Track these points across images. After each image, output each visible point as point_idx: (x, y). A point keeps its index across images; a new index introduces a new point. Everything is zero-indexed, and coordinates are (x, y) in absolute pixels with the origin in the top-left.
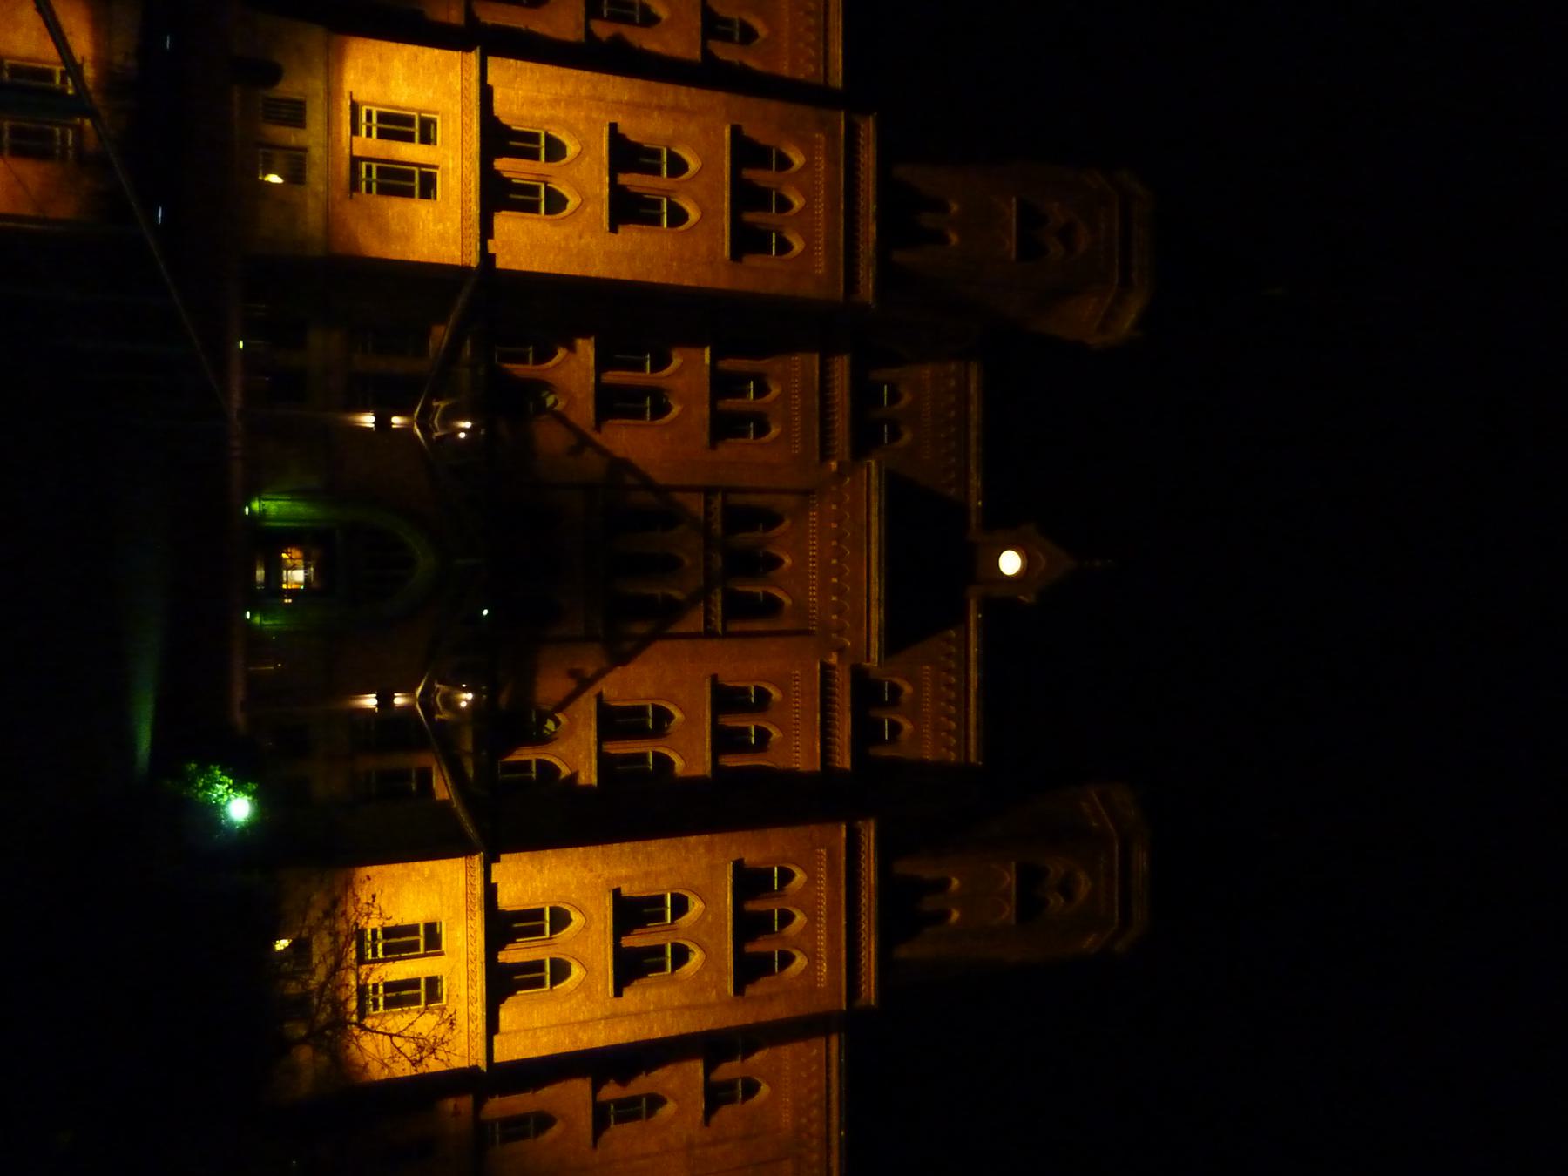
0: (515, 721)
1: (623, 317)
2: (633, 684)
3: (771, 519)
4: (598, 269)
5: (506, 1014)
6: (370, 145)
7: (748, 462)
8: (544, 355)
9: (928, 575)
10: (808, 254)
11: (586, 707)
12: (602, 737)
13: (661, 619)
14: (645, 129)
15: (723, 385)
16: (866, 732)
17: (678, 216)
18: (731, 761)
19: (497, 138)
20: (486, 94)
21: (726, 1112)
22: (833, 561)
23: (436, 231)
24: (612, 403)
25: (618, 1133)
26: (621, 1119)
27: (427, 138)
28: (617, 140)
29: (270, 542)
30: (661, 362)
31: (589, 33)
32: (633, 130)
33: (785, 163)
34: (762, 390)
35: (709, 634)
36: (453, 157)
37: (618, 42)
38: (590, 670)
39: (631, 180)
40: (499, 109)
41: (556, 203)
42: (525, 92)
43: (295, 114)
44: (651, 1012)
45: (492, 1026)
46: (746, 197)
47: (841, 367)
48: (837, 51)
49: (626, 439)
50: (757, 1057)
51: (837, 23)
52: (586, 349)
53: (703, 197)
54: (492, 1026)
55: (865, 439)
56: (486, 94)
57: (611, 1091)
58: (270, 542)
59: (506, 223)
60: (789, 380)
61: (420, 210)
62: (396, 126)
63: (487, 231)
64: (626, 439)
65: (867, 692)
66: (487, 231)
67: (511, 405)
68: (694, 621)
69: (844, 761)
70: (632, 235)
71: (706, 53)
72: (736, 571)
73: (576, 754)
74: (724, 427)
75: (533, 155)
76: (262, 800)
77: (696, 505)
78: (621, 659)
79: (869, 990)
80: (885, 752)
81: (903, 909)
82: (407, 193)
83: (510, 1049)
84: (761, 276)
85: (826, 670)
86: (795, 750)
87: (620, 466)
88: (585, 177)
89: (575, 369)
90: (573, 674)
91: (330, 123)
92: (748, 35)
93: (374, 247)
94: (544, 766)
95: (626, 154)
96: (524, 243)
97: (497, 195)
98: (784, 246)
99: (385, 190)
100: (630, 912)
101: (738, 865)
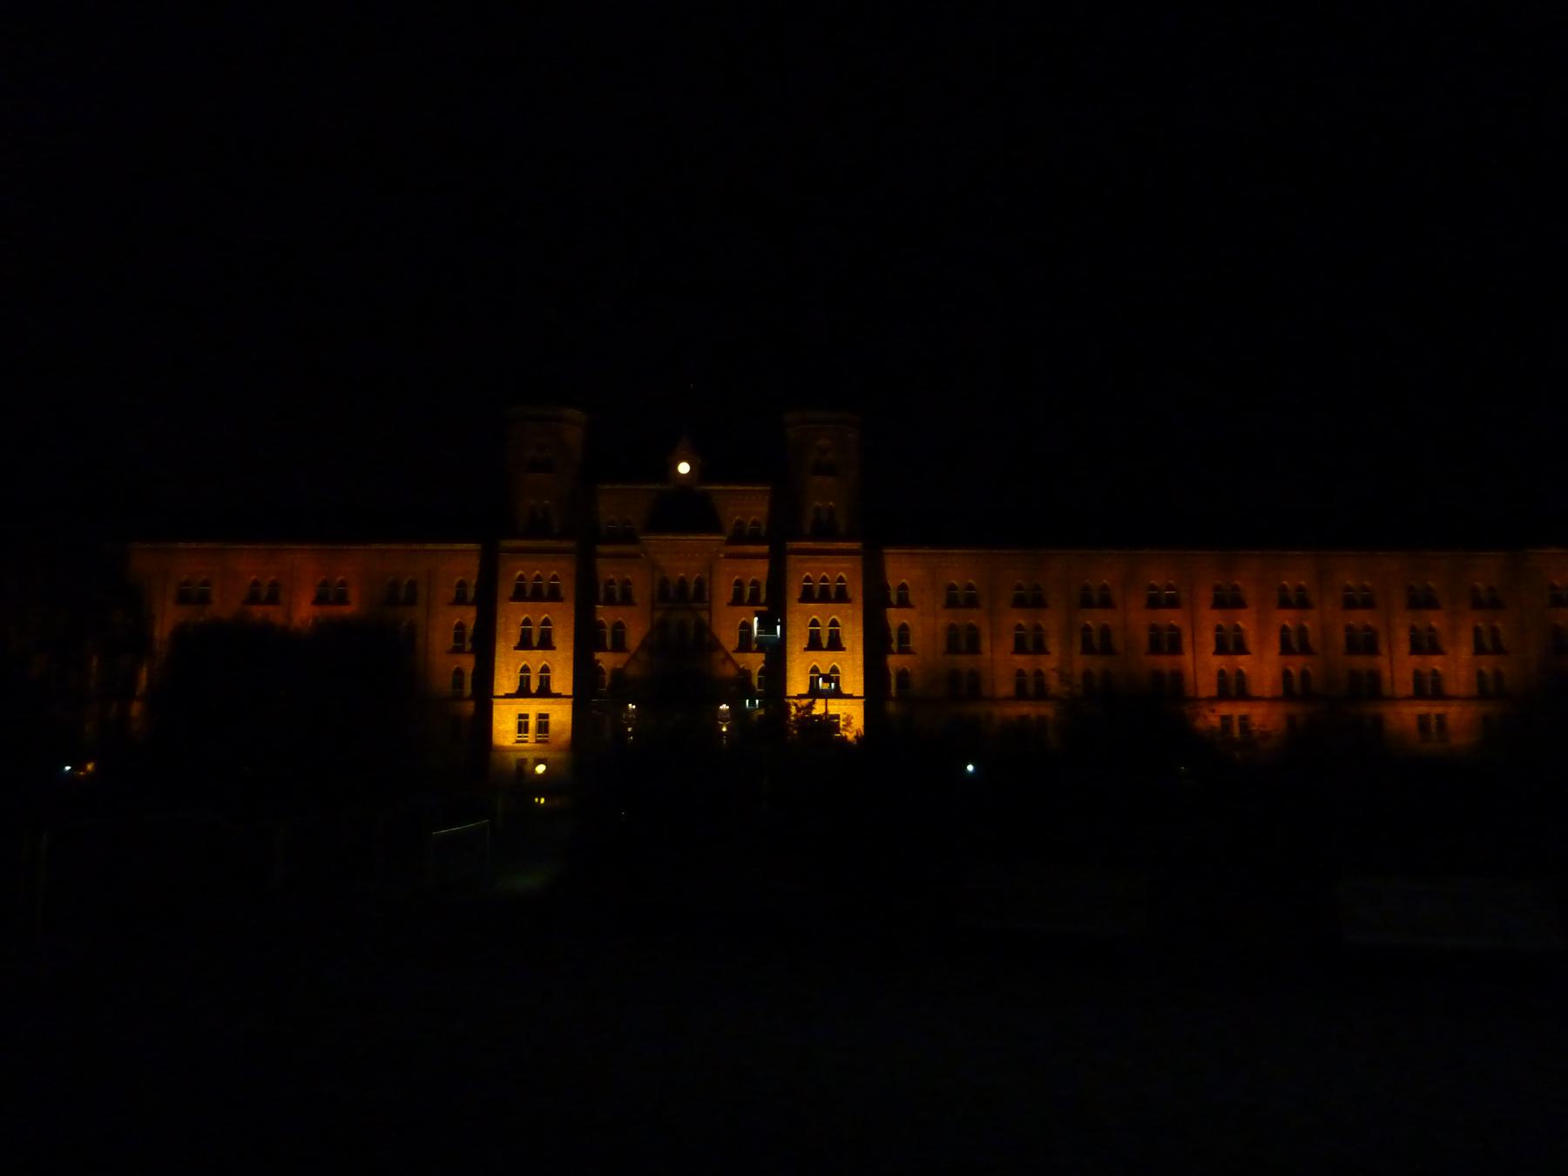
0: (740, 686)
1: (587, 642)
2: (728, 638)
3: (664, 582)
4: (570, 654)
5: (846, 691)
6: (531, 736)
7: (642, 590)
8: (601, 671)
9: (687, 512)
10: (558, 570)
11: (737, 657)
12: (750, 651)
13: (703, 629)
14: (514, 634)
15: (610, 601)
16: (754, 539)
17: (546, 622)
18: (763, 597)
19: (523, 692)
20: (507, 696)
21: (912, 598)
22: (679, 555)
23: (560, 715)
24: (619, 646)
25: (913, 644)
26: (907, 641)
27: (525, 716)
28: (518, 648)
29: (672, 722)
30: (602, 625)
31: (470, 652)
32: (515, 641)
33: (521, 578)
34: (611, 582)
35: (709, 610)
36: (533, 708)
37: (474, 639)
38: (722, 656)
39: (535, 640)
40: (513, 691)
41: (545, 669)
42: (505, 682)
43: (523, 761)
44: (853, 637)
45: (850, 697)
46: (537, 596)
47: (603, 549)
48: (464, 546)
49: (634, 638)
50: (890, 583)
51: (458, 546)
52: (598, 656)
53: (537, 612)
54: (850, 697)
55: (629, 537)
56: (507, 696)
57: (894, 646)
58: (672, 722)
59: (555, 688)
60: (607, 571)
61: (552, 719)
62: (523, 727)
63: (558, 696)
64: (634, 638)
65: (738, 537)
66: (558, 696)
67: (622, 685)
68: (704, 615)
69: (765, 549)
70: (557, 640)
71: (472, 604)
72: (683, 601)
73: (755, 662)
74: (627, 599)
75: (528, 678)
76: (89, 761)
77: (658, 615)
78: (716, 645)
79: (856, 546)
80: (764, 528)
81: (825, 531)
82: (547, 724)
83: (859, 690)
84: (567, 587)
85: (728, 556)
86: (759, 570)
87: (644, 645)
88: (535, 659)
89: (606, 661)
90: (723, 662)
91: (525, 750)
92: (462, 584)
93: (567, 735)
94: (760, 673)
95: (525, 644)
96: (562, 682)
97: (545, 692)
98: (555, 578)
99: (546, 731)
100: (814, 644)
101: (801, 600)
